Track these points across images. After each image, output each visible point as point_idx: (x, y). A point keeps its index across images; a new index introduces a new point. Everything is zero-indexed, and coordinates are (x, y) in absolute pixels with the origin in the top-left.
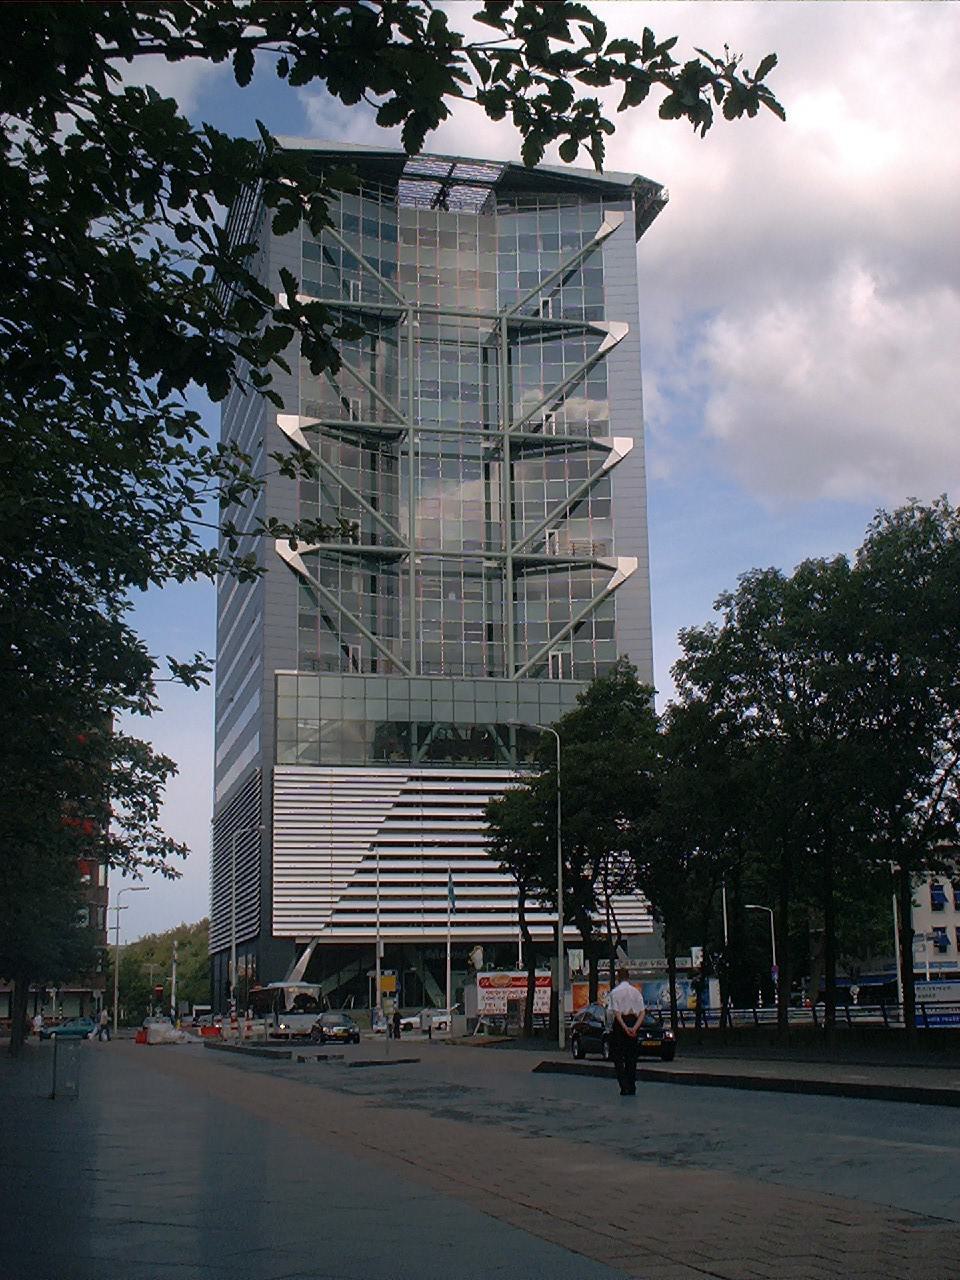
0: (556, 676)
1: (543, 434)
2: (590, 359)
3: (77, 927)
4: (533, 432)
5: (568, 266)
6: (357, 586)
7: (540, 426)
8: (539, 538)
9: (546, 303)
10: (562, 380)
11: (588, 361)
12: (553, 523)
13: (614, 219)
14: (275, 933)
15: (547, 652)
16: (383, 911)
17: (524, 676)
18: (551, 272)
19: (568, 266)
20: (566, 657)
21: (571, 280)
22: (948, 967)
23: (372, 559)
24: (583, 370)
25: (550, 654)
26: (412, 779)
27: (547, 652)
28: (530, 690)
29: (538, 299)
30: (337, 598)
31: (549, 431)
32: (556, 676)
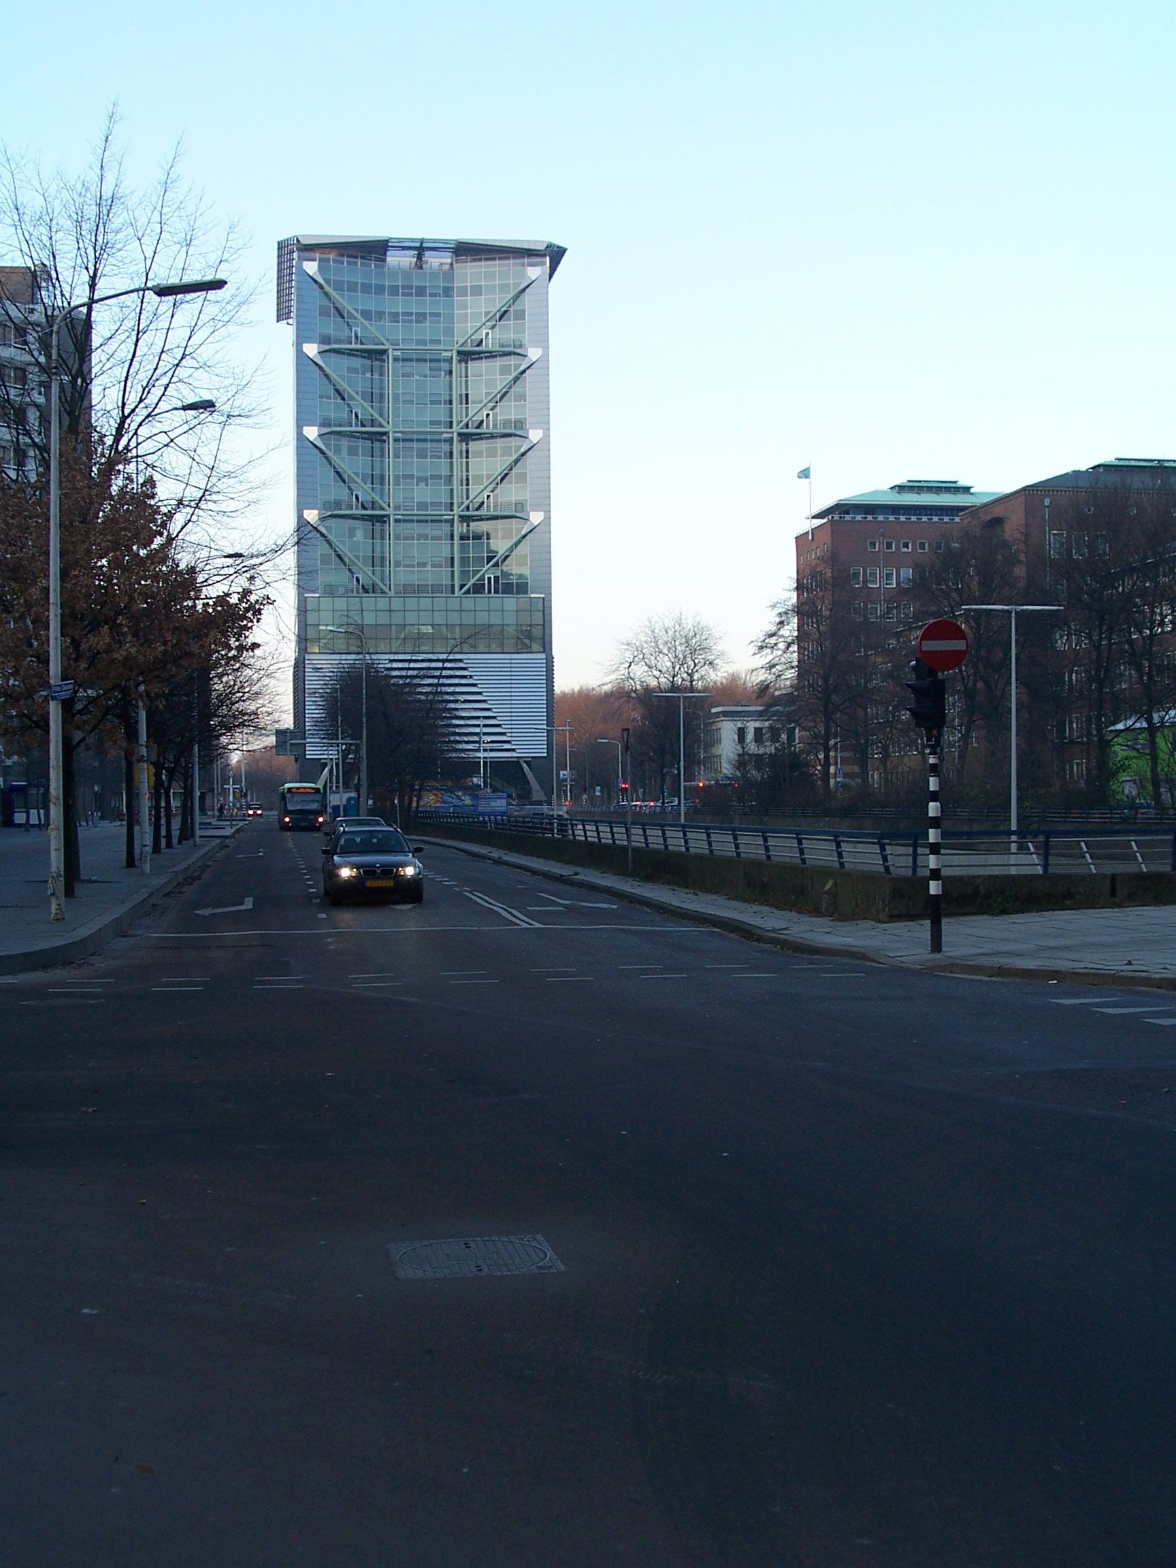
0: (490, 592)
1: (483, 348)
2: (516, 374)
3: (16, 757)
4: (476, 428)
5: (502, 307)
6: (359, 535)
7: (482, 341)
8: (479, 500)
9: (488, 415)
10: (497, 470)
11: (514, 375)
12: (491, 487)
13: (534, 272)
14: (307, 757)
15: (484, 575)
16: (485, 726)
17: (468, 592)
18: (491, 312)
19: (502, 307)
20: (496, 578)
21: (505, 399)
22: (627, 767)
23: (372, 519)
24: (510, 382)
25: (486, 576)
26: (392, 661)
27: (484, 575)
28: (468, 603)
29: (483, 413)
30: (359, 561)
31: (488, 427)
32: (490, 592)
